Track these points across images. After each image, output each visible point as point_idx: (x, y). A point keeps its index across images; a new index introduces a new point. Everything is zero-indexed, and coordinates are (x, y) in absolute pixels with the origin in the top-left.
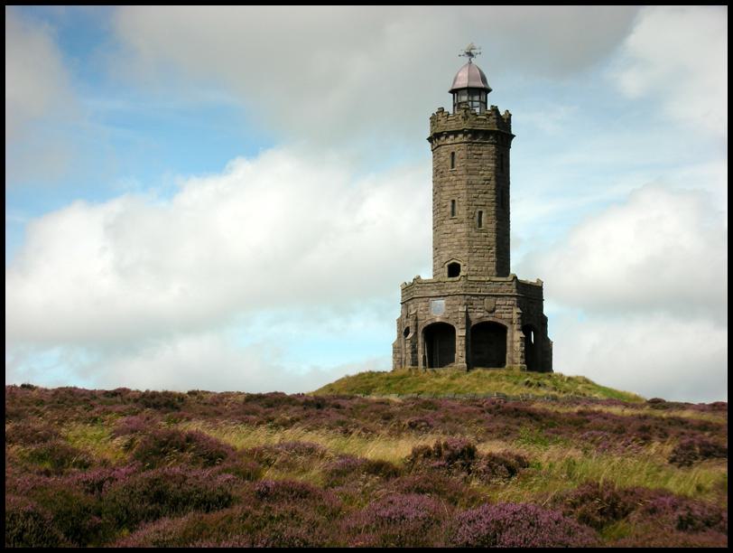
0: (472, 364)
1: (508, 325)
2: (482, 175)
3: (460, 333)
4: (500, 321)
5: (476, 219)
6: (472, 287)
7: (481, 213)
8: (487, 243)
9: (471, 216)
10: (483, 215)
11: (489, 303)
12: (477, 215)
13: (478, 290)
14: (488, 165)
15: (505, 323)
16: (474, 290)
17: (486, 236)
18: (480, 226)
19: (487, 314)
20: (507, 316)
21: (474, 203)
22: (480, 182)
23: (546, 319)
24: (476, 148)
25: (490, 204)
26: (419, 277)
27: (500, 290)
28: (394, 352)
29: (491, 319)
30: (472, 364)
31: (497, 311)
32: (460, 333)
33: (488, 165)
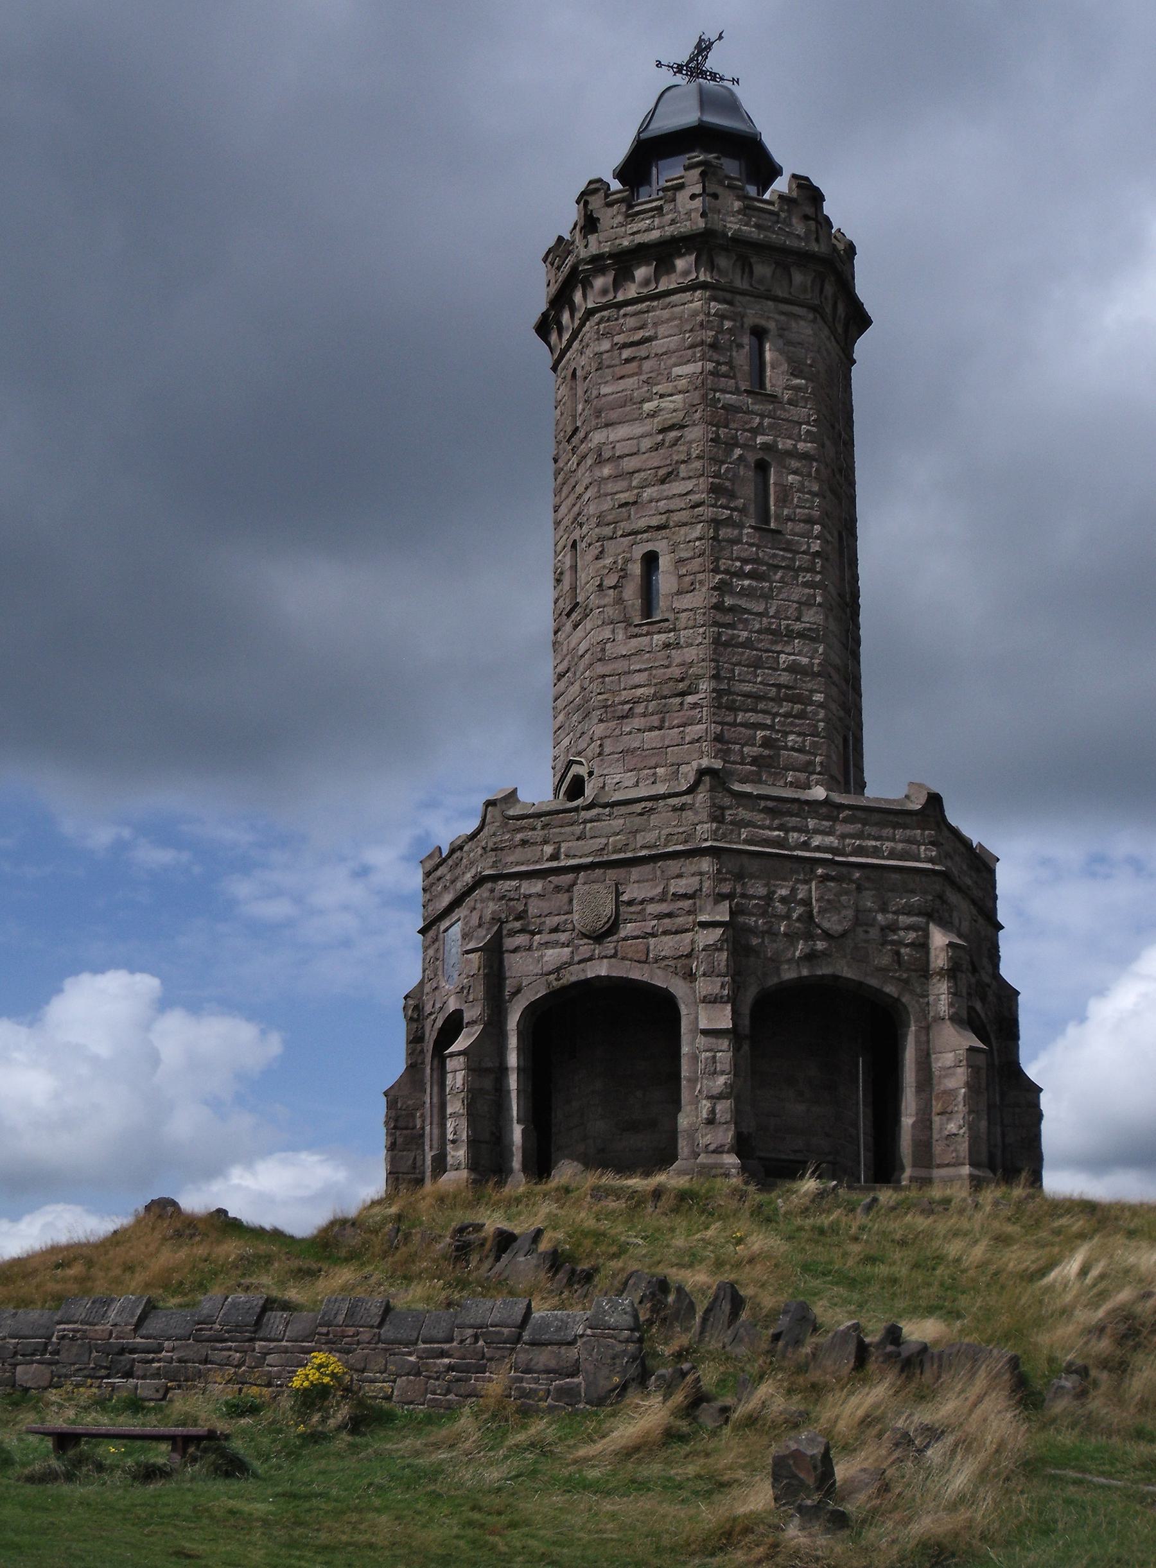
0: (767, 1162)
1: (678, 988)
2: (653, 415)
3: (705, 1019)
4: (637, 973)
5: (631, 592)
6: (524, 843)
7: (650, 560)
8: (676, 672)
9: (611, 580)
10: (664, 562)
11: (592, 900)
12: (636, 569)
13: (549, 850)
14: (677, 371)
15: (658, 979)
16: (529, 853)
17: (667, 646)
18: (648, 608)
19: (586, 948)
20: (666, 945)
21: (626, 526)
22: (646, 443)
23: (1012, 994)
24: (631, 322)
25: (683, 516)
26: (511, 797)
27: (640, 839)
28: (409, 1042)
29: (602, 969)
30: (767, 1162)
31: (627, 929)
32: (705, 1019)
33: (677, 371)
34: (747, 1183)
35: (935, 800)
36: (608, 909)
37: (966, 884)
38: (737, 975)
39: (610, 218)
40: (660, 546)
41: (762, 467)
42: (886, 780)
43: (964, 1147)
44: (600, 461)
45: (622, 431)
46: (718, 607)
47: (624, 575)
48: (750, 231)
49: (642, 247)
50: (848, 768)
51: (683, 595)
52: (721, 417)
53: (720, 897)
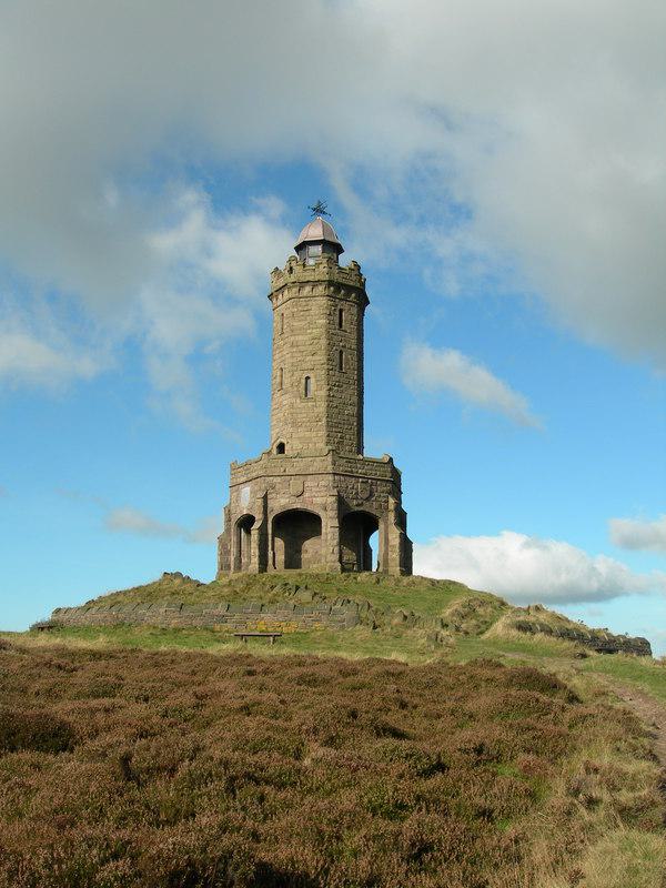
1: (322, 514)
10: (312, 380)
12: (303, 381)
34: (545, 548)
35: (391, 459)
36: (301, 489)
37: (394, 482)
38: (339, 509)
39: (298, 269)
40: (311, 375)
41: (341, 352)
42: (374, 449)
43: (398, 562)
44: (292, 346)
45: (300, 337)
46: (329, 396)
47: (300, 382)
48: (340, 280)
49: (345, 285)
50: (360, 449)
51: (319, 389)
52: (330, 337)
53: (334, 487)
